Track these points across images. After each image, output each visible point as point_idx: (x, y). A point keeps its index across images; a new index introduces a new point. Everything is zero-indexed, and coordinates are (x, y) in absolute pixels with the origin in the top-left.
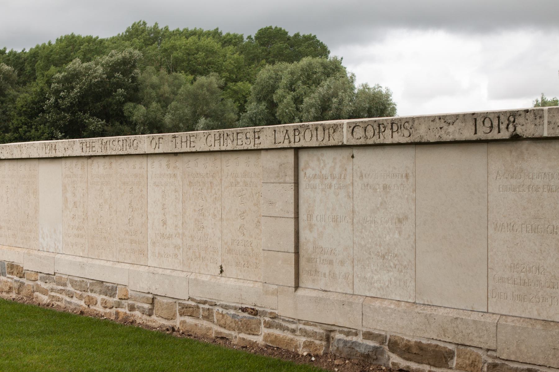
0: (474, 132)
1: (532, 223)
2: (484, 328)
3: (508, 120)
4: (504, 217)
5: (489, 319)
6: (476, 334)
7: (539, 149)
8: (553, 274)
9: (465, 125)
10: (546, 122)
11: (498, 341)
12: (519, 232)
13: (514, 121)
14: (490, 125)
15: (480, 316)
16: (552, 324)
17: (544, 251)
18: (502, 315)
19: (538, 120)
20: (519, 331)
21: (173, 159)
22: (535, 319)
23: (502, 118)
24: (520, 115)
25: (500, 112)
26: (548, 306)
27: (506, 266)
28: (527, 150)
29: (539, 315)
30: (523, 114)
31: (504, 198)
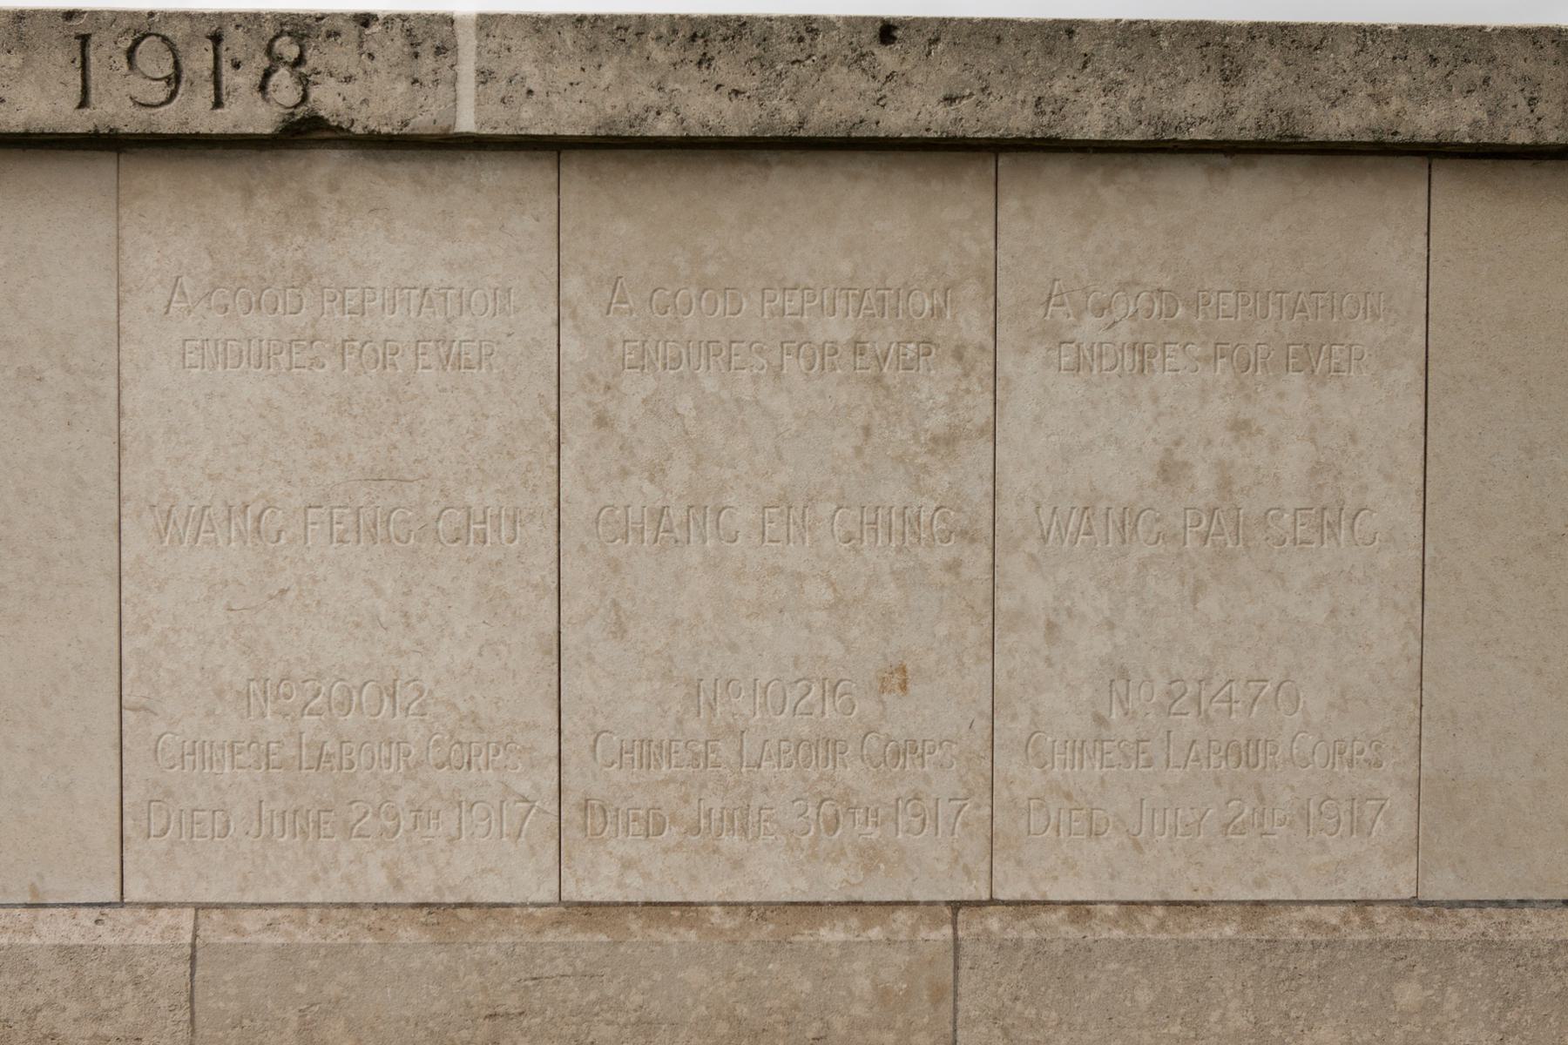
0: (76, 97)
1: (363, 501)
2: (122, 975)
3: (269, 51)
4: (210, 477)
5: (147, 933)
6: (74, 1008)
7: (398, 187)
8: (464, 708)
9: (26, 62)
10: (467, 67)
11: (201, 1019)
12: (291, 541)
13: (300, 61)
14: (168, 70)
15: (90, 923)
16: (465, 914)
17: (421, 619)
18: (199, 907)
19: (428, 62)
20: (314, 964)
21: (625, 222)
22: (376, 906)
23: (235, 42)
24: (334, 34)
25: (220, 16)
26: (442, 843)
27: (220, 694)
28: (333, 187)
29: (398, 885)
30: (352, 31)
31: (210, 396)
